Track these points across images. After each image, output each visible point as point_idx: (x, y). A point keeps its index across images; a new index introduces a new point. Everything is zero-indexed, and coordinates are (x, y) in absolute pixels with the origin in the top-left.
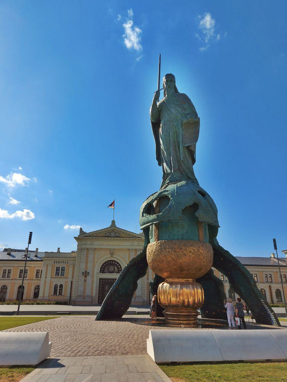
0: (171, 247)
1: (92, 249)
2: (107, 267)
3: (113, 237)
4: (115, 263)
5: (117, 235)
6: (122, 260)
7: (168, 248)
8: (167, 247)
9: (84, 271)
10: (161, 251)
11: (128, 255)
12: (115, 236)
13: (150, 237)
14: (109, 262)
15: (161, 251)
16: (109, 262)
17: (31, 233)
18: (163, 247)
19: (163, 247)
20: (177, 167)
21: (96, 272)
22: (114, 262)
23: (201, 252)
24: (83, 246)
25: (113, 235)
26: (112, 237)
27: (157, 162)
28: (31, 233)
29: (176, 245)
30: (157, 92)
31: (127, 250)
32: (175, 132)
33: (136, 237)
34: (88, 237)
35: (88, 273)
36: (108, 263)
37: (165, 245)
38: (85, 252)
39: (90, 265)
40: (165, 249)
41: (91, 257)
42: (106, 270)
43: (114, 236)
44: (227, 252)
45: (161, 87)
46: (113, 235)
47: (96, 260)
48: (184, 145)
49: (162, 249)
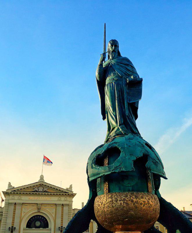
0: (122, 199)
1: (19, 204)
2: (34, 221)
3: (41, 192)
4: (39, 217)
5: (45, 190)
6: (48, 215)
7: (120, 201)
8: (119, 199)
9: (11, 226)
10: (112, 204)
11: (54, 210)
12: (43, 190)
13: (97, 189)
14: (36, 217)
15: (112, 204)
16: (36, 217)
17: (105, 24)
18: (114, 199)
19: (114, 199)
20: (122, 122)
21: (22, 228)
22: (38, 217)
23: (151, 205)
24: (10, 201)
25: (41, 189)
26: (39, 192)
27: (102, 117)
28: (105, 24)
29: (127, 197)
30: (103, 54)
31: (54, 205)
32: (120, 90)
33: (64, 193)
34: (16, 191)
35: (15, 228)
36: (42, 218)
37: (116, 197)
38: (12, 207)
39: (17, 221)
40: (117, 201)
41: (18, 211)
42: (32, 224)
43: (42, 191)
44: (170, 204)
45: (107, 51)
46: (41, 189)
47: (23, 215)
48: (128, 102)
49: (114, 201)
